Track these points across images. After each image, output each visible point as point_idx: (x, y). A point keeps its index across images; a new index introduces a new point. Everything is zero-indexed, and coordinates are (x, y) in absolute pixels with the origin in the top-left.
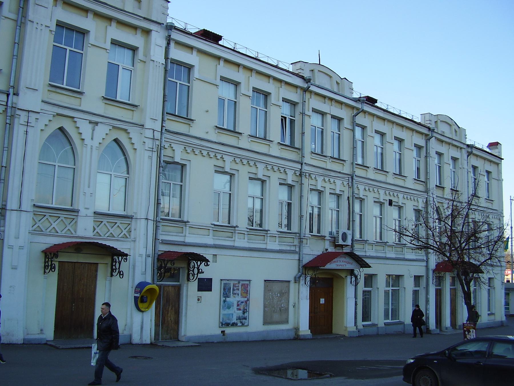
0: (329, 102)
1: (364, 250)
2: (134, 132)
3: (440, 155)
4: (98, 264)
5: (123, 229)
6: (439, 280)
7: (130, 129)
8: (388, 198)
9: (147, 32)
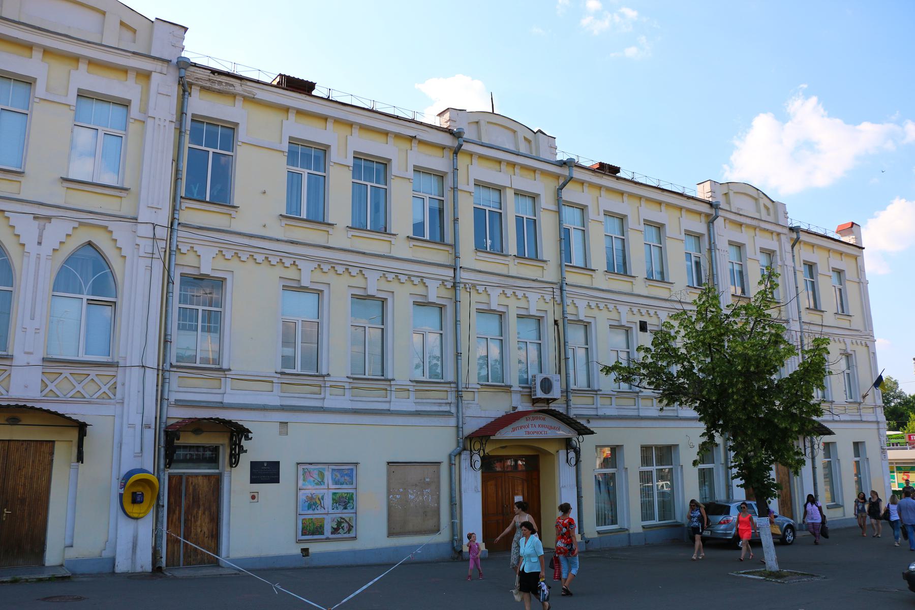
0: (510, 169)
1: (594, 406)
2: (120, 231)
4: (53, 442)
5: (102, 385)
7: (112, 226)
8: (638, 319)
9: (146, 75)
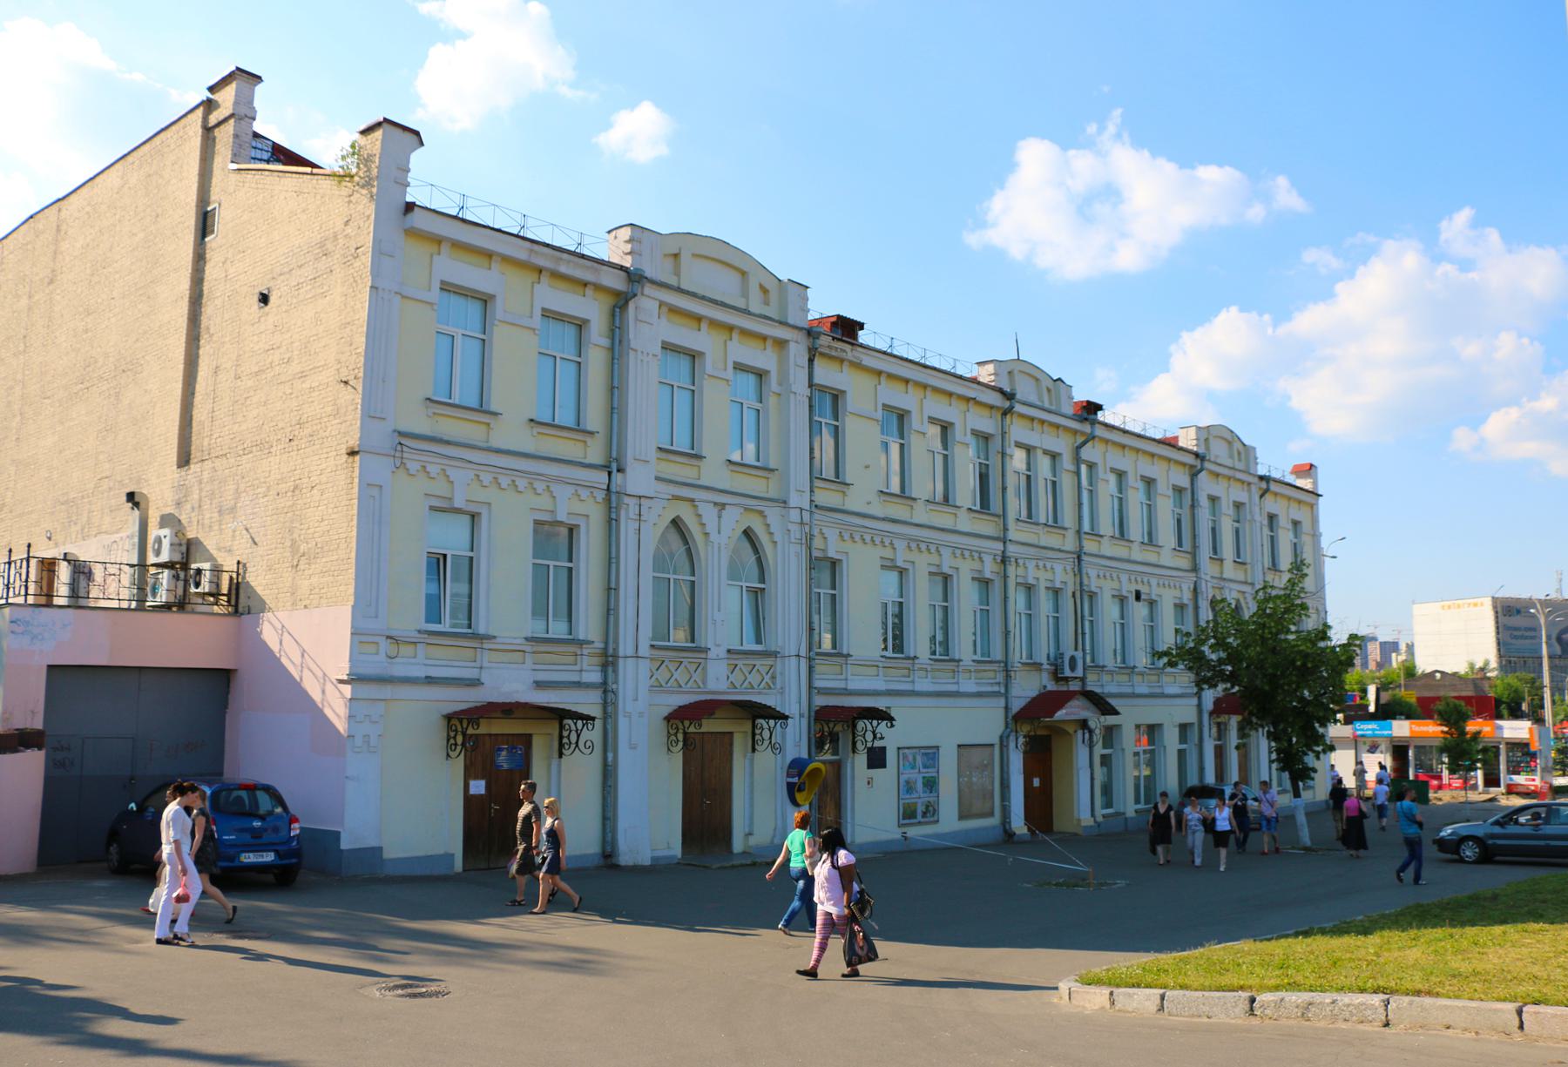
2: (773, 514)
3: (1213, 499)
6: (1222, 730)
8: (1133, 588)
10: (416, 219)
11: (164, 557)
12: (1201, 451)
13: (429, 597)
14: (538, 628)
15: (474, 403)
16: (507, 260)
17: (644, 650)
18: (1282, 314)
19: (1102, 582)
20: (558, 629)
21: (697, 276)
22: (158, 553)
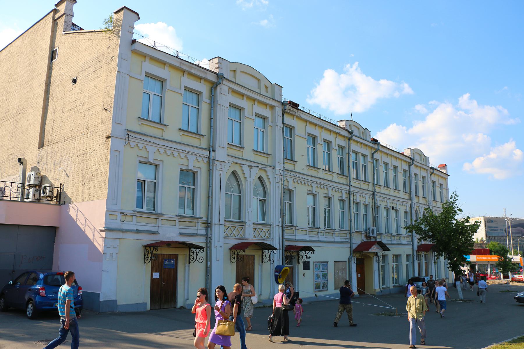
0: (391, 157)
2: (270, 171)
3: (416, 175)
8: (391, 205)
10: (135, 46)
11: (32, 183)
12: (412, 157)
13: (138, 197)
14: (181, 212)
15: (157, 120)
16: (172, 66)
17: (222, 222)
18: (410, 126)
19: (381, 203)
20: (189, 213)
21: (242, 79)
22: (29, 181)
